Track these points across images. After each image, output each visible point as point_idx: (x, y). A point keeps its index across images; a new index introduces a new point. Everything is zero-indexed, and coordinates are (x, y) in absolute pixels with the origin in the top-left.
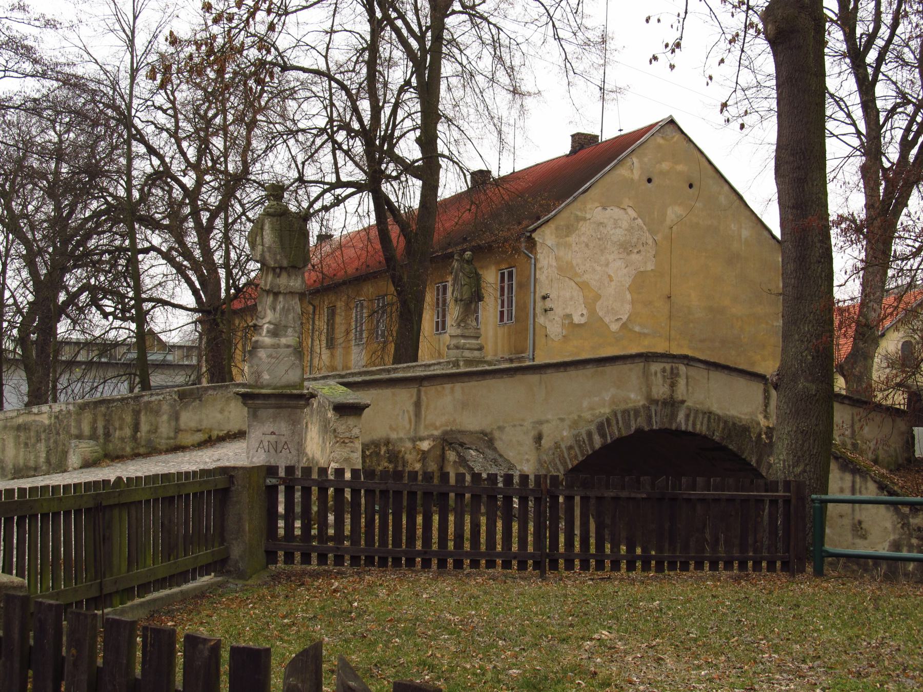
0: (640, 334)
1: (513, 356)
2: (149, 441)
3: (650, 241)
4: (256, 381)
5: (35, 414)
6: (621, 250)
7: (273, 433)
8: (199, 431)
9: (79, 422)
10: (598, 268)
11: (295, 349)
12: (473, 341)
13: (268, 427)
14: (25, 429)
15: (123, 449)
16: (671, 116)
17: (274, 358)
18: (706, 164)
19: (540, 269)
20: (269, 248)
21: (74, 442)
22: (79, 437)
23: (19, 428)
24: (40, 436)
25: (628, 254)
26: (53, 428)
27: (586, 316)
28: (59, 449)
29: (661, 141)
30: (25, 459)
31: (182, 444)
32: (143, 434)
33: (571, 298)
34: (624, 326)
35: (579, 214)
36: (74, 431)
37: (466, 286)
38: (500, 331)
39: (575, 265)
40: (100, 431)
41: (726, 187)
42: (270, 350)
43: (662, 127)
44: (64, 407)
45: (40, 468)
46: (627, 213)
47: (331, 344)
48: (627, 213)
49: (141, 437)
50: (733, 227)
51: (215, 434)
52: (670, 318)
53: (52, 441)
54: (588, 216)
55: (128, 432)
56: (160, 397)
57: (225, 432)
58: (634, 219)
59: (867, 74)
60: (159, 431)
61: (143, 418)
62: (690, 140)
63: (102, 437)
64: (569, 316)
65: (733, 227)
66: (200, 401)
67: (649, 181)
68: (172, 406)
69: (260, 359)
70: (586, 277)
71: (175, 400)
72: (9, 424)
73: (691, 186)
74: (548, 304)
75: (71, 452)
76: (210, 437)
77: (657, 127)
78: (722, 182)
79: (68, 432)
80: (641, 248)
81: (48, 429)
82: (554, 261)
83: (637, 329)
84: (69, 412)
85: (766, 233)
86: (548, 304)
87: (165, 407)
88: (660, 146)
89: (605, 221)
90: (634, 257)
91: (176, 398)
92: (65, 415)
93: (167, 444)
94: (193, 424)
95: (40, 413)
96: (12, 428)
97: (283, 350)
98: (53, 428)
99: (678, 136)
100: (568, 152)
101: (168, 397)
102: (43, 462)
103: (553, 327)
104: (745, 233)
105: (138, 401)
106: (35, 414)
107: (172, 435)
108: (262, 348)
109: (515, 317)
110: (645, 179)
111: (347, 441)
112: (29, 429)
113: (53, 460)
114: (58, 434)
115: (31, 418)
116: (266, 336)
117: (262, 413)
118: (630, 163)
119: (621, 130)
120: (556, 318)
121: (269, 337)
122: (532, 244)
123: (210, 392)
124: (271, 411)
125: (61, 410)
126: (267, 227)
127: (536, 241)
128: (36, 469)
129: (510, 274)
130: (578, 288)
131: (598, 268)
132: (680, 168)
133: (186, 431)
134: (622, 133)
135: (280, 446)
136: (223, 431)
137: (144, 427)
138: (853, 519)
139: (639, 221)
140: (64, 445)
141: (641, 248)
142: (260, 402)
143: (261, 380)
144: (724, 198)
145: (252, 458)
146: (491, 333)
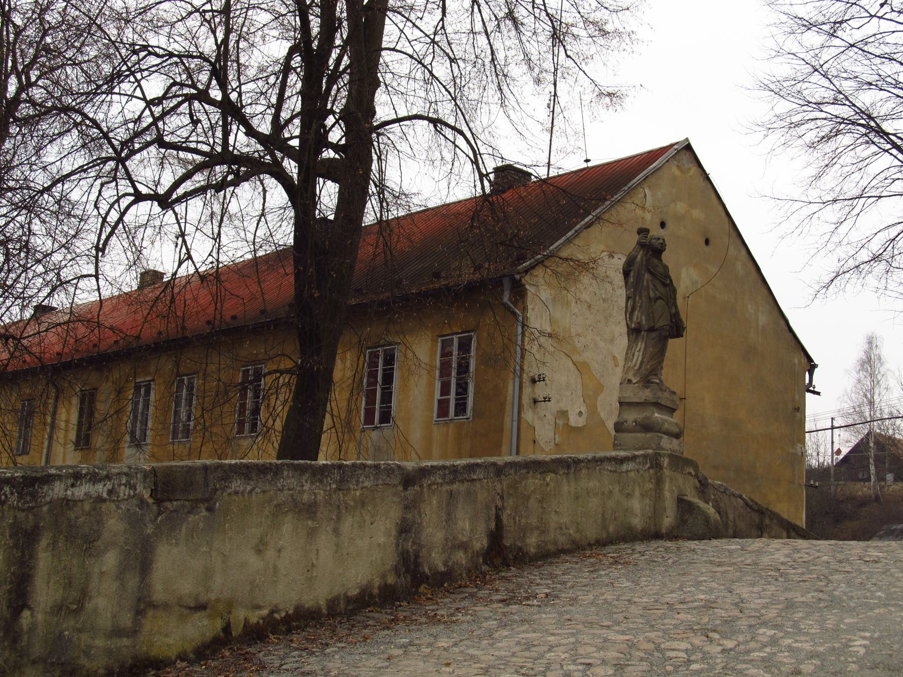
2: (58, 642)
8: (201, 607)
10: (602, 344)
16: (687, 139)
18: (723, 214)
27: (585, 416)
29: (677, 172)
31: (154, 652)
32: (40, 617)
37: (659, 301)
38: (437, 433)
39: (573, 334)
41: (744, 252)
43: (679, 152)
49: (33, 628)
50: (751, 308)
51: (241, 616)
56: (101, 489)
57: (265, 612)
60: (89, 606)
61: (44, 559)
64: (563, 414)
65: (751, 308)
66: (210, 509)
68: (134, 522)
70: (587, 356)
71: (142, 502)
73: (707, 242)
74: (540, 391)
76: (227, 629)
77: (672, 152)
78: (739, 242)
82: (548, 324)
85: (782, 322)
91: (146, 495)
93: (109, 652)
94: (187, 587)
99: (694, 169)
101: (124, 492)
104: (763, 319)
105: (34, 496)
107: (126, 620)
109: (474, 409)
110: (658, 222)
118: (642, 195)
119: (587, 161)
120: (549, 416)
122: (519, 292)
123: (237, 484)
127: (526, 290)
129: (464, 346)
130: (576, 371)
131: (602, 344)
132: (697, 213)
133: (166, 606)
134: (590, 164)
136: (259, 607)
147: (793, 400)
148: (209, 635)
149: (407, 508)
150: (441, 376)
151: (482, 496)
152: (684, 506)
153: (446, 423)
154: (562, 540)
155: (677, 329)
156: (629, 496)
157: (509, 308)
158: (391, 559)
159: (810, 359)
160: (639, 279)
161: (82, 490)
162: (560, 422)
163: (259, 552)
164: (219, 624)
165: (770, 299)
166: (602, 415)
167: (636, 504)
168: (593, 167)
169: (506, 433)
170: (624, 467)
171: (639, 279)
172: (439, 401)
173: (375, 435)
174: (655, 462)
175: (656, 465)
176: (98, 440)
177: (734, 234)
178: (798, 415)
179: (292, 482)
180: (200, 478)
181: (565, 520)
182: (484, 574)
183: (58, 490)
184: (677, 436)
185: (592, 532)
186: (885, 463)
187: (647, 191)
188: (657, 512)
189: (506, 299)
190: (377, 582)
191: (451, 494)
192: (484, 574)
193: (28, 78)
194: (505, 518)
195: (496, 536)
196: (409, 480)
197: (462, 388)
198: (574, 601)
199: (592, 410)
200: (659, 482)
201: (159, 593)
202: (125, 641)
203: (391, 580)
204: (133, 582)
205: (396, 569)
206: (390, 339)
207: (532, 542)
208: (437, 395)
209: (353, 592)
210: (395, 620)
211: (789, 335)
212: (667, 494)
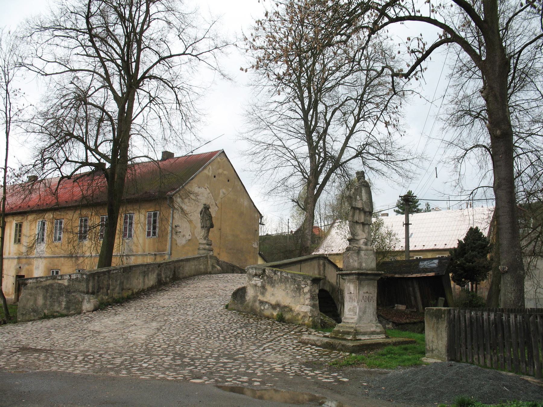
3: (214, 204)
7: (367, 292)
13: (365, 289)
18: (234, 172)
20: (365, 202)
33: (186, 227)
41: (240, 183)
52: (220, 238)
58: (209, 193)
65: (242, 200)
67: (215, 177)
73: (228, 181)
77: (218, 154)
78: (239, 180)
88: (219, 162)
99: (225, 159)
103: (181, 241)
106: (58, 279)
110: (213, 176)
129: (155, 215)
135: (370, 298)
144: (239, 187)
155: (212, 226)
159: (261, 215)
166: (196, 235)
168: (194, 155)
171: (203, 216)
179: (141, 268)
197: (154, 228)
199: (193, 234)
208: (147, 230)
211: (254, 208)
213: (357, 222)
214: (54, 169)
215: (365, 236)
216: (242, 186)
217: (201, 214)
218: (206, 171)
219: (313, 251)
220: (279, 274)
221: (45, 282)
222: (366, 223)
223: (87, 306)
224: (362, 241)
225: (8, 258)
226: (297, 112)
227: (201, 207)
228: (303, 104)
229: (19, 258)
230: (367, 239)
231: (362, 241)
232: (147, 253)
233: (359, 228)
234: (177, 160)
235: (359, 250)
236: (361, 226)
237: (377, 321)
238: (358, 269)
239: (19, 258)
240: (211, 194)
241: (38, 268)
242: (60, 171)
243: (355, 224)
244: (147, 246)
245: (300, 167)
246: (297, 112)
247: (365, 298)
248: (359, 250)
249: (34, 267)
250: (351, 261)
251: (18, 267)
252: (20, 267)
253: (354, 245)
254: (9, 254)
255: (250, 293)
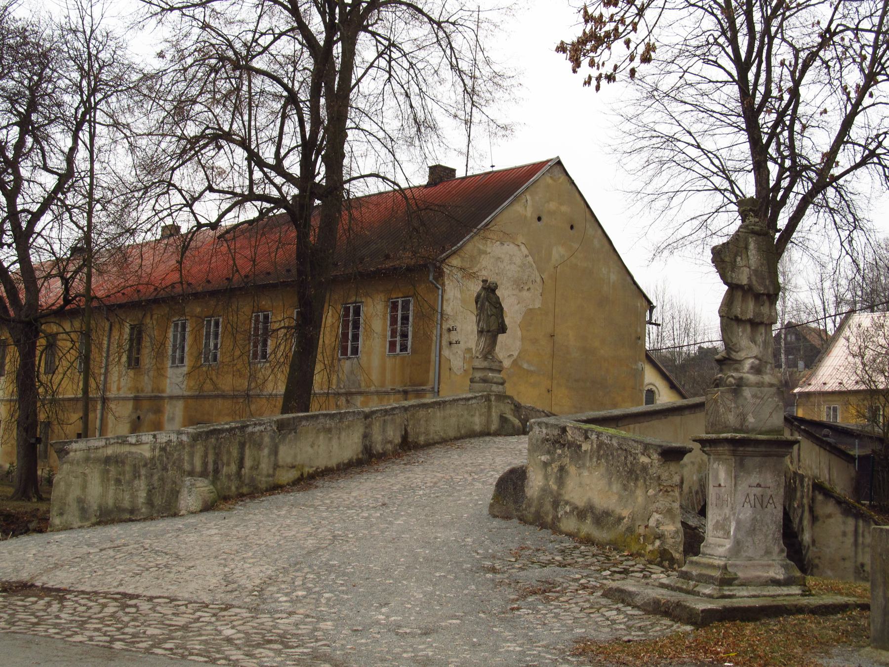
0: (528, 371)
1: (409, 388)
3: (538, 279)
4: (742, 425)
5: (131, 444)
6: (515, 286)
7: (759, 485)
8: (293, 467)
9: (192, 455)
11: (778, 389)
12: (497, 375)
13: (754, 479)
14: (117, 462)
15: (229, 488)
16: (558, 157)
17: (758, 398)
19: (447, 300)
20: (756, 271)
21: (188, 480)
22: (191, 474)
23: (107, 460)
24: (139, 472)
25: (520, 291)
26: (158, 463)
28: (166, 488)
29: (550, 181)
30: (116, 499)
31: (280, 482)
34: (515, 363)
35: (481, 247)
36: (187, 467)
38: (389, 363)
40: (211, 467)
41: (600, 231)
42: (755, 389)
43: (551, 167)
44: (174, 437)
45: (138, 510)
46: (520, 250)
47: (134, 363)
48: (520, 250)
50: (604, 270)
51: (307, 470)
52: (553, 356)
53: (156, 477)
54: (489, 250)
55: (233, 468)
56: (262, 428)
58: (526, 256)
59: (761, 139)
61: (247, 452)
62: (573, 183)
63: (211, 474)
65: (604, 270)
67: (539, 219)
68: (272, 438)
69: (746, 399)
72: (92, 456)
73: (572, 227)
74: (454, 337)
75: (185, 492)
76: (302, 475)
77: (547, 167)
79: (180, 468)
80: (531, 286)
81: (149, 464)
83: (525, 366)
84: (181, 443)
85: (628, 278)
86: (454, 337)
87: (267, 440)
89: (503, 256)
90: (525, 294)
92: (175, 447)
93: (267, 482)
94: (289, 460)
95: (139, 443)
96: (97, 460)
97: (766, 389)
98: (158, 463)
99: (563, 177)
100: (425, 183)
101: (269, 428)
102: (143, 503)
104: (613, 277)
106: (131, 444)
107: (271, 472)
108: (747, 386)
111: (669, 489)
112: (123, 463)
113: (158, 501)
114: (165, 469)
115: (125, 449)
116: (748, 373)
117: (749, 462)
120: (459, 352)
121: (751, 373)
123: (304, 423)
124: (757, 459)
125: (170, 441)
126: (752, 246)
127: (444, 272)
128: (132, 512)
129: (406, 307)
132: (564, 208)
133: (283, 467)
134: (495, 169)
135: (766, 500)
137: (248, 463)
138: (856, 561)
139: (530, 258)
140: (174, 483)
141: (531, 286)
142: (750, 449)
143: (747, 424)
145: (739, 514)
146: (376, 362)
147: (636, 331)
148: (296, 477)
149: (366, 427)
150: (391, 325)
151: (398, 421)
152: (503, 419)
153: (394, 356)
154: (437, 438)
155: (503, 329)
156: (472, 416)
157: (433, 283)
158: (360, 448)
160: (483, 305)
161: (257, 428)
162: (467, 356)
163: (312, 447)
164: (299, 473)
165: (620, 263)
167: (477, 419)
169: (432, 363)
170: (470, 402)
171: (483, 305)
172: (390, 342)
173: (348, 363)
174: (488, 398)
175: (488, 398)
176: (147, 359)
177: (593, 220)
178: (640, 342)
179: (323, 420)
180: (292, 422)
181: (438, 429)
182: (399, 454)
183: (250, 429)
184: (502, 384)
185: (452, 433)
186: (799, 350)
187: (528, 197)
188: (489, 422)
189: (431, 278)
190: (355, 457)
191: (384, 421)
192: (399, 454)
193: (90, 103)
194: (409, 429)
195: (405, 438)
196: (367, 416)
198: (432, 463)
200: (489, 408)
201: (281, 463)
202: (271, 479)
203: (360, 456)
204: (273, 458)
205: (362, 452)
206: (359, 299)
207: (422, 439)
208: (389, 339)
209: (346, 461)
210: (362, 471)
211: (634, 287)
212: (494, 414)
213: (737, 320)
214: (179, 207)
215: (755, 351)
216: (605, 240)
217: (477, 303)
218: (518, 208)
219: (797, 386)
220: (594, 437)
221: (105, 449)
222: (757, 320)
223: (189, 500)
224: (747, 365)
225: (115, 399)
226: (720, 66)
227: (475, 287)
228: (736, 50)
229: (136, 399)
230: (760, 360)
231: (747, 365)
232: (389, 388)
233: (743, 332)
234: (460, 183)
235: (740, 384)
236: (749, 328)
237: (785, 554)
238: (736, 430)
239: (136, 399)
240: (530, 257)
241: (172, 419)
242: (193, 212)
243: (734, 323)
244: (388, 376)
245: (733, 192)
246: (720, 66)
247: (752, 498)
248: (740, 384)
249: (166, 417)
250: (722, 410)
251: (134, 416)
252: (139, 418)
253: (730, 374)
254: (119, 389)
255: (535, 483)
